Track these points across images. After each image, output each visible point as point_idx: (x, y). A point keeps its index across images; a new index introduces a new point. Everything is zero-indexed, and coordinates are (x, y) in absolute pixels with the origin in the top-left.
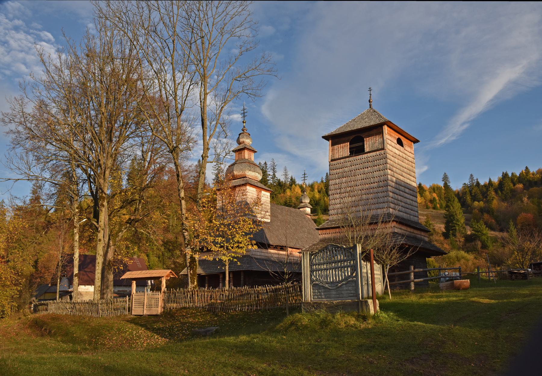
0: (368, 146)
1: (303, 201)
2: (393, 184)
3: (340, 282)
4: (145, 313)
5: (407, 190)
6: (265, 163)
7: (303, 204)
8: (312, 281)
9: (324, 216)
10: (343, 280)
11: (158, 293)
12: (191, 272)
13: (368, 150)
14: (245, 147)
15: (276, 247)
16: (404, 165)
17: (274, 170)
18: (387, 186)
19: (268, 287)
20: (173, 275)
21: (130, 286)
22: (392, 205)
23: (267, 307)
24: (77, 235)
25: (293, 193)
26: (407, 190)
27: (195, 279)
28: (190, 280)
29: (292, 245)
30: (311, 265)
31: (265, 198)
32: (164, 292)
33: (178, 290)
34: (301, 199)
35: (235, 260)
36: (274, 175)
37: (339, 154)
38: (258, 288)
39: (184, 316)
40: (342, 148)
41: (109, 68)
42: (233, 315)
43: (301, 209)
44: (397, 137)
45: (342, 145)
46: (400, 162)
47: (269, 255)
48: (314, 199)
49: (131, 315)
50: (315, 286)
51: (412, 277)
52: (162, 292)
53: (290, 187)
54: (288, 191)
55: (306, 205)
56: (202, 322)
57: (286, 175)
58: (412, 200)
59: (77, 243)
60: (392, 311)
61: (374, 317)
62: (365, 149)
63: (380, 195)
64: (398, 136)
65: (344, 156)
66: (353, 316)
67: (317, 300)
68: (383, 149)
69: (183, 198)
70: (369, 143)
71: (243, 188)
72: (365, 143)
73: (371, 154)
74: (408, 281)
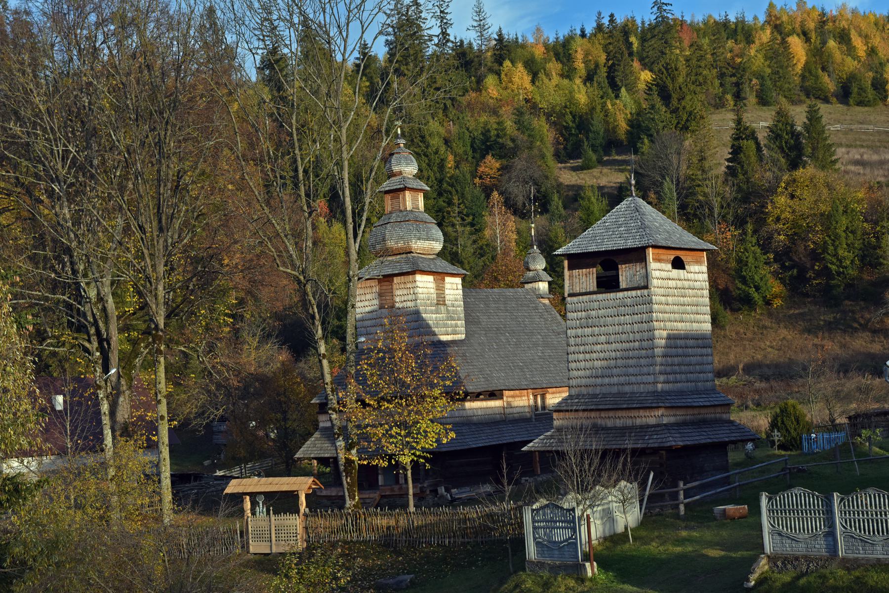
0: (624, 278)
1: (532, 267)
7: (531, 274)
8: (535, 539)
9: (605, 170)
10: (564, 541)
11: (294, 517)
12: (348, 480)
13: (624, 287)
14: (406, 187)
15: (477, 396)
17: (442, 18)
18: (653, 348)
19: (479, 508)
24: (105, 402)
25: (506, 88)
27: (355, 491)
28: (347, 494)
30: (534, 521)
31: (452, 292)
33: (329, 512)
34: (528, 263)
35: (422, 460)
36: (444, 34)
37: (581, 286)
38: (464, 509)
40: (584, 276)
43: (527, 286)
44: (672, 257)
45: (584, 270)
48: (573, 109)
50: (538, 544)
51: (682, 496)
52: (301, 514)
54: (490, 81)
55: (538, 275)
56: (381, 565)
57: (481, 27)
58: (701, 355)
59: (108, 418)
60: (613, 571)
61: (591, 580)
62: (621, 284)
63: (643, 361)
64: (671, 255)
65: (588, 290)
66: (573, 578)
68: (646, 287)
70: (626, 274)
72: (620, 273)
73: (629, 293)
74: (676, 502)
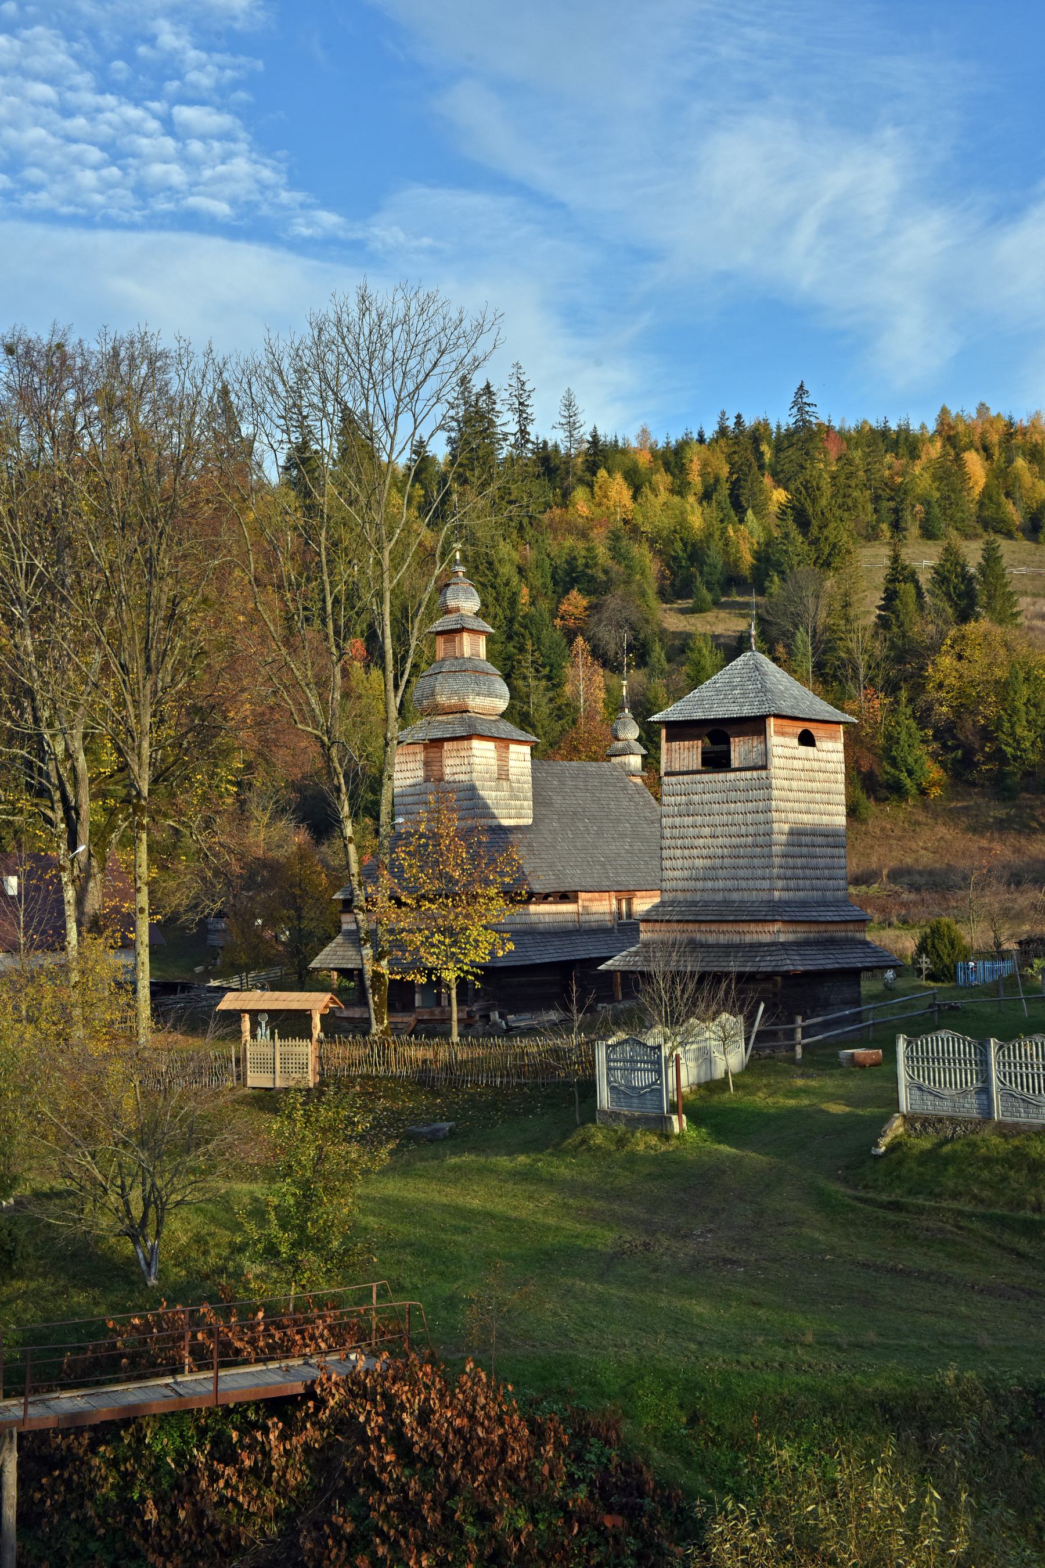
1: (621, 735)
2: (784, 837)
3: (642, 1088)
4: (279, 1084)
5: (820, 840)
6: (488, 387)
8: (609, 1082)
16: (815, 786)
20: (335, 1002)
21: (239, 1020)
22: (780, 884)
23: (540, 1081)
25: (600, 505)
26: (820, 840)
28: (373, 1016)
29: (588, 882)
30: (609, 1060)
32: (320, 1041)
39: (370, 1094)
41: (499, 1080)
42: (471, 1095)
43: (614, 760)
44: (800, 731)
46: (802, 784)
47: (534, 919)
49: (245, 1085)
50: (612, 1089)
53: (588, 477)
54: (580, 494)
55: (629, 746)
57: (571, 425)
59: (72, 908)
60: (706, 1126)
61: (678, 1137)
67: (616, 1109)
68: (764, 767)
69: (351, 840)
70: (739, 749)
71: (465, 744)
